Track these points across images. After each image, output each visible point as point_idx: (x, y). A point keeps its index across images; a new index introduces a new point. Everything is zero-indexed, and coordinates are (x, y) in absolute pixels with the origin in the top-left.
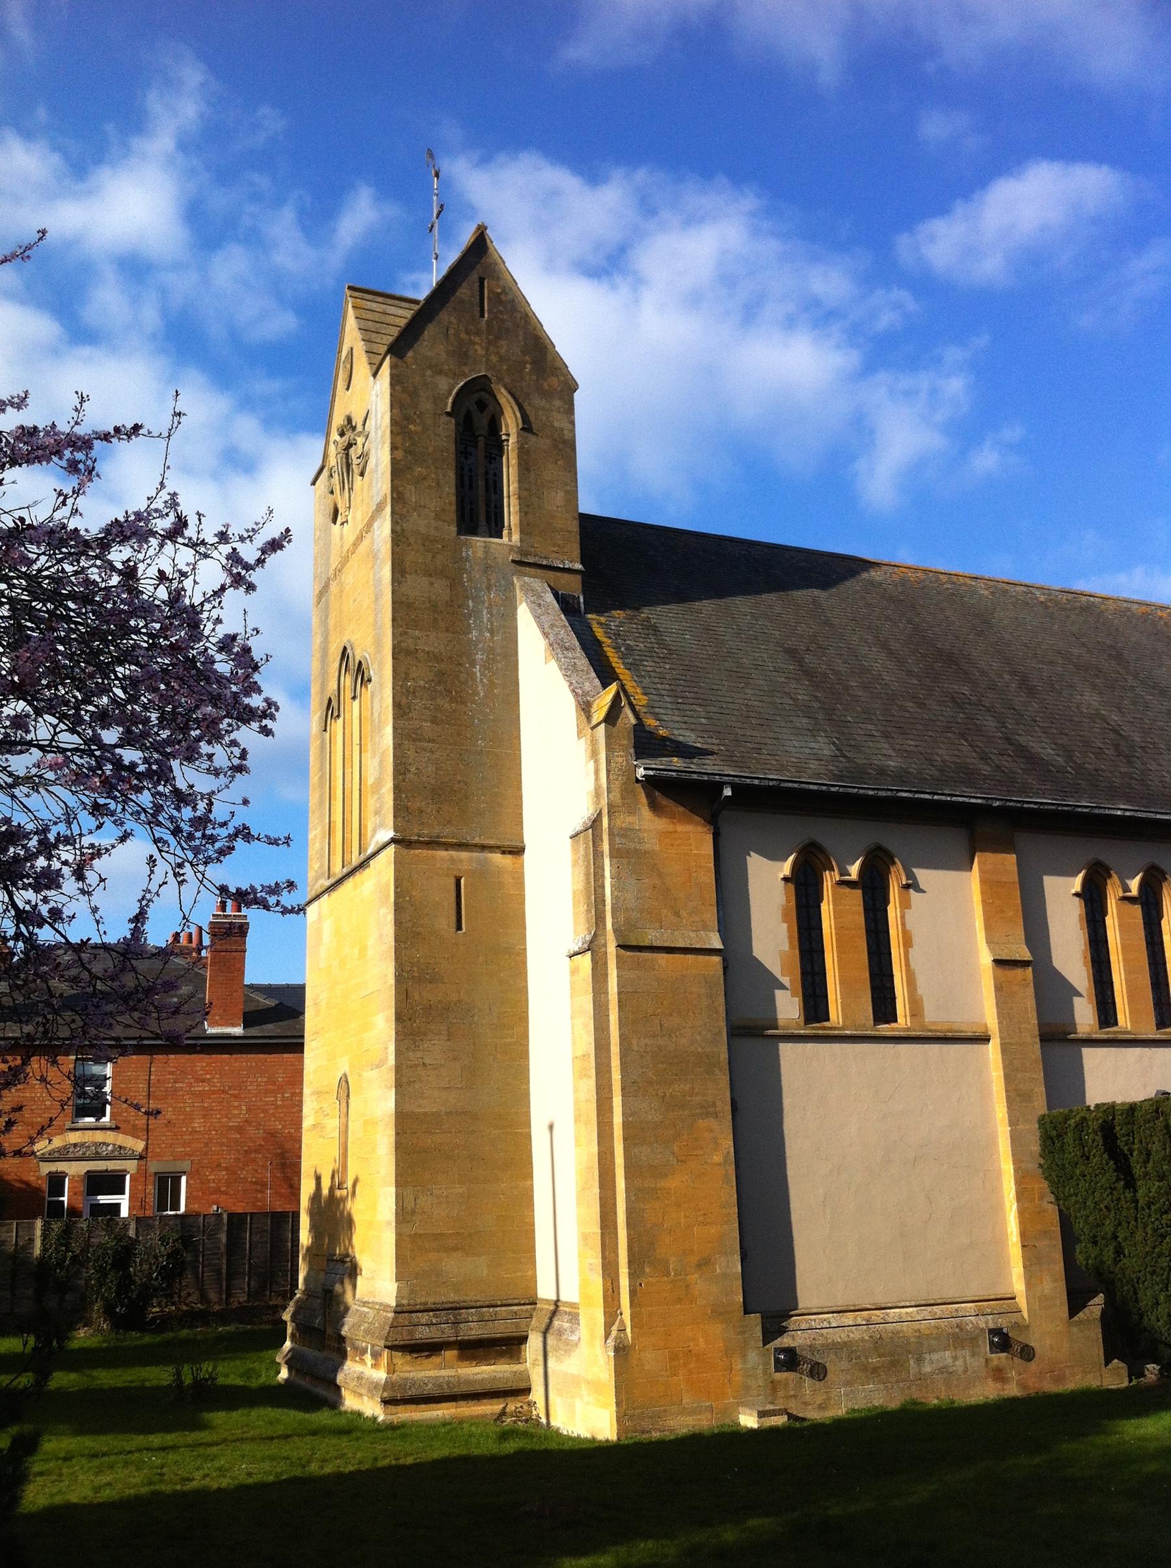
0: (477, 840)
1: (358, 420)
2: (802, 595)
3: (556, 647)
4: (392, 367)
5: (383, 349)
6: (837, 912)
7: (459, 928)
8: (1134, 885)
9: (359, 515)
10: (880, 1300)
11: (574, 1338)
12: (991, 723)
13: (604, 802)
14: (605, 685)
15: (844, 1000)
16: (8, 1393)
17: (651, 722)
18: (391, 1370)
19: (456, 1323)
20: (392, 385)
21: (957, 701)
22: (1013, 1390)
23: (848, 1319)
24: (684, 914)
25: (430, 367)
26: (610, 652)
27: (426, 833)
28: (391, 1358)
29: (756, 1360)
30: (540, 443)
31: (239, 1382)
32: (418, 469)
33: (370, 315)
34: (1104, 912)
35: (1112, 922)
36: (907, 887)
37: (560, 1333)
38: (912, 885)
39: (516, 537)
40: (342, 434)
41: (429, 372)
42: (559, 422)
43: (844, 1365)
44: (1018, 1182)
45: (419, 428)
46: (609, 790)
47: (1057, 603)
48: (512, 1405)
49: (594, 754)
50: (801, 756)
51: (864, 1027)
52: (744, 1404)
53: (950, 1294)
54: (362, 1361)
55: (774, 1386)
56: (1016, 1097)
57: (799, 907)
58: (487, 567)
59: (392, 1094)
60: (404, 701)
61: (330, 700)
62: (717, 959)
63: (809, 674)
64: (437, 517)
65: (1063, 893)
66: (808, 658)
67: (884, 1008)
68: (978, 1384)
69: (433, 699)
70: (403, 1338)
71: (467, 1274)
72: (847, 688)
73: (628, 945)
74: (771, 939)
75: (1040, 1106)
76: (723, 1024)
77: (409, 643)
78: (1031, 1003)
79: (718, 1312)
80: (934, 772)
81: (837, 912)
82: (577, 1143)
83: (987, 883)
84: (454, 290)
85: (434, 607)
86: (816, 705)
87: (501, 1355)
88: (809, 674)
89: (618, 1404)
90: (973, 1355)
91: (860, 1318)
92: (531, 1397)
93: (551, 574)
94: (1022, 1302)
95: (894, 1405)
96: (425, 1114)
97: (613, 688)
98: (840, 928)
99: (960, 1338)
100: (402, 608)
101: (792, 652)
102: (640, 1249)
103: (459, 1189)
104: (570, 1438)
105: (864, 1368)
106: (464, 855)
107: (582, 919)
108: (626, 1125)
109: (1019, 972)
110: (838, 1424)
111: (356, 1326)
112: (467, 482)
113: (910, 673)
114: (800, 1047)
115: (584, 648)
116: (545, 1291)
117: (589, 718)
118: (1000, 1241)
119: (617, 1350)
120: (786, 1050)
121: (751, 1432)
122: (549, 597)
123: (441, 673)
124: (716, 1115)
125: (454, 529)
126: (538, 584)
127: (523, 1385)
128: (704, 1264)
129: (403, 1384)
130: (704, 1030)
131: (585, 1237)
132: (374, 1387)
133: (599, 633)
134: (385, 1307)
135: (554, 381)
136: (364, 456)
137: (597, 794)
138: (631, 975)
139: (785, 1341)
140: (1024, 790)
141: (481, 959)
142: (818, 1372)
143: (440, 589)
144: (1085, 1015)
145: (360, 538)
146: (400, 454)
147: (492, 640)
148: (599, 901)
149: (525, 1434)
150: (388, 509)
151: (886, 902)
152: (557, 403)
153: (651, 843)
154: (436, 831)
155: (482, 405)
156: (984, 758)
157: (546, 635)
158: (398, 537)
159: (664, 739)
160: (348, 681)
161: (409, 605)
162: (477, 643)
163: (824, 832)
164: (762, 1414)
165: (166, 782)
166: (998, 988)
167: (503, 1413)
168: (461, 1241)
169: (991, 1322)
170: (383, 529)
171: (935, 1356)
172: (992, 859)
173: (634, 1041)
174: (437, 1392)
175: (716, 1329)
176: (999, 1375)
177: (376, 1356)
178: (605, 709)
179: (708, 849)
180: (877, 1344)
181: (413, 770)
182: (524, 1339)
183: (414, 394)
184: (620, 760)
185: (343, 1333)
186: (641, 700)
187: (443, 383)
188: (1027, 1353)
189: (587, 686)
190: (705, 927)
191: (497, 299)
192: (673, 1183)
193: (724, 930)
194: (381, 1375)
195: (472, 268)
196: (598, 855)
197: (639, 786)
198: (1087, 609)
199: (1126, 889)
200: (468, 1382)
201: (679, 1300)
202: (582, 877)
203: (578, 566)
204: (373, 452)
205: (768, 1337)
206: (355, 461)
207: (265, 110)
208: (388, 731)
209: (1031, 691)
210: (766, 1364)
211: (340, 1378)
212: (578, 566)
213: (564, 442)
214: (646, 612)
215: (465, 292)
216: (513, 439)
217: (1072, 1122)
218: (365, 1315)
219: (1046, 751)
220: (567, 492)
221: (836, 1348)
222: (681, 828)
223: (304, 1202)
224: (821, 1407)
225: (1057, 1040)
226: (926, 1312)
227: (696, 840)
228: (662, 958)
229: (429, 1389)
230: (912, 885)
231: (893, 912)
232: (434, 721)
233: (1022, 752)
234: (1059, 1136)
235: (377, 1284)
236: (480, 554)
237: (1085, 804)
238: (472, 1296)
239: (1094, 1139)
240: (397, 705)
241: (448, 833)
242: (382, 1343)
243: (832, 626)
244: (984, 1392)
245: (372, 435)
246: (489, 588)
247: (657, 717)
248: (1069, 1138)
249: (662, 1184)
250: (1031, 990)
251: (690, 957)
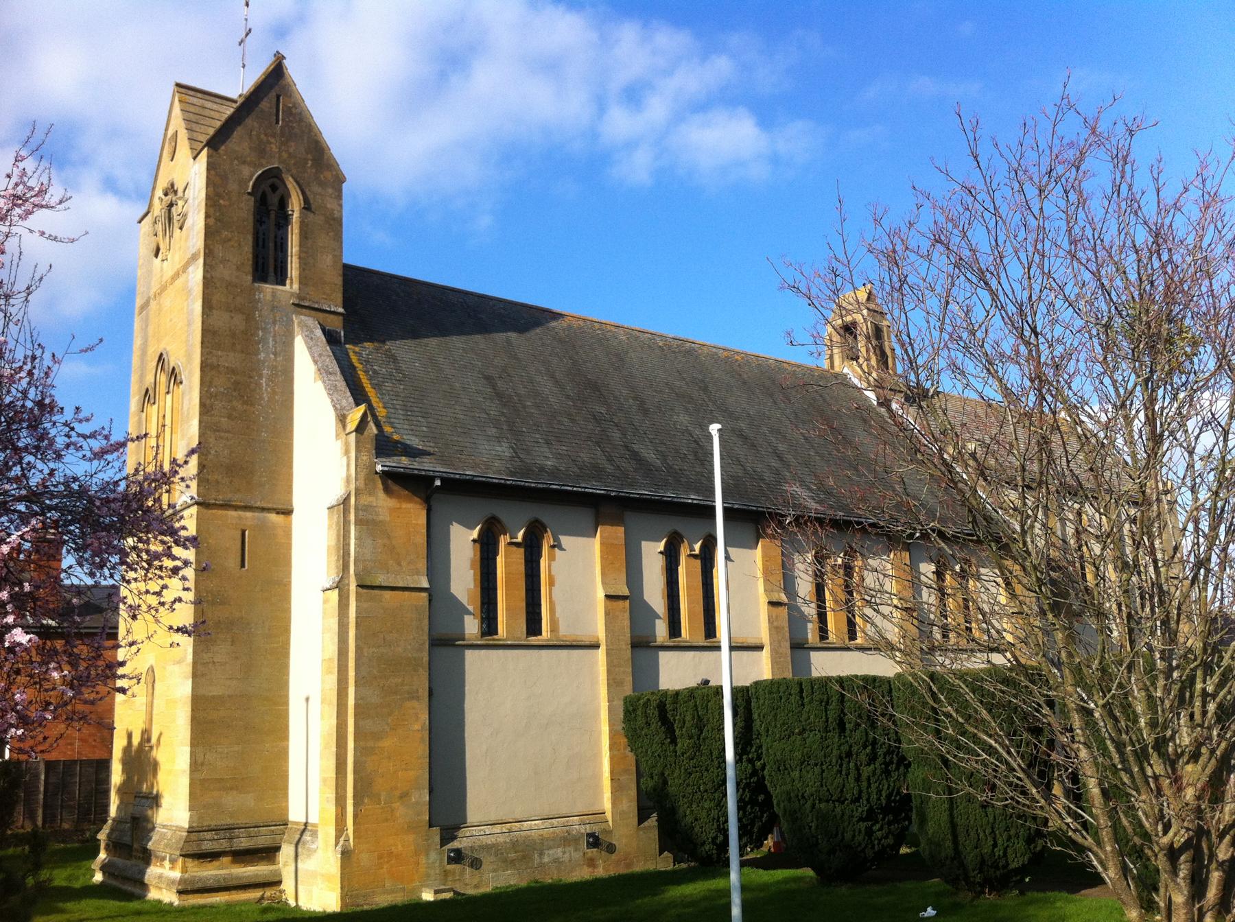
0: (258, 504)
1: (180, 187)
2: (500, 337)
3: (323, 372)
4: (209, 156)
5: (204, 138)
6: (507, 563)
7: (243, 565)
8: (697, 547)
9: (177, 258)
10: (518, 817)
11: (314, 846)
12: (616, 435)
13: (353, 487)
14: (357, 404)
15: (508, 620)
17: (388, 429)
18: (184, 870)
19: (231, 839)
20: (208, 170)
21: (596, 418)
22: (600, 872)
23: (497, 829)
24: (404, 564)
25: (237, 158)
26: (362, 375)
27: (221, 498)
28: (184, 863)
29: (435, 857)
30: (316, 219)
31: (64, 884)
32: (225, 233)
33: (192, 109)
34: (677, 564)
35: (682, 570)
36: (553, 547)
37: (304, 843)
38: (557, 546)
39: (296, 286)
40: (166, 194)
41: (236, 162)
42: (331, 204)
43: (492, 858)
44: (611, 738)
45: (227, 203)
46: (356, 479)
47: (670, 347)
48: (269, 893)
49: (347, 452)
50: (490, 459)
51: (520, 639)
52: (427, 886)
53: (564, 811)
54: (162, 865)
55: (446, 874)
56: (613, 683)
57: (482, 559)
58: (273, 308)
59: (190, 682)
60: (208, 402)
61: (147, 390)
62: (425, 595)
63: (499, 395)
64: (238, 269)
65: (652, 553)
66: (500, 383)
67: (534, 625)
68: (578, 868)
69: (230, 401)
70: (193, 849)
71: (237, 805)
72: (524, 407)
73: (364, 585)
74: (463, 581)
75: (628, 690)
76: (426, 638)
78: (627, 623)
79: (411, 828)
80: (576, 470)
81: (507, 563)
82: (322, 718)
83: (606, 547)
84: (257, 103)
85: (233, 335)
86: (503, 419)
87: (262, 859)
88: (499, 395)
89: (342, 888)
90: (576, 850)
91: (505, 828)
92: (282, 887)
93: (320, 315)
94: (609, 815)
95: (523, 884)
96: (213, 697)
97: (362, 408)
98: (508, 574)
99: (568, 840)
100: (209, 335)
101: (488, 378)
102: (362, 786)
103: (236, 748)
104: (308, 912)
105: (505, 861)
106: (249, 514)
107: (333, 566)
108: (357, 706)
109: (621, 603)
110: (485, 898)
111: (159, 842)
112: (261, 244)
113: (568, 397)
114: (477, 652)
115: (343, 372)
116: (296, 814)
117: (344, 426)
118: (597, 776)
119: (343, 853)
120: (470, 655)
121: (429, 903)
122: (319, 332)
123: (237, 383)
124: (418, 698)
125: (250, 278)
126: (311, 322)
127: (277, 879)
128: (404, 796)
129: (192, 881)
130: (412, 642)
131: (324, 780)
132: (172, 882)
133: (354, 359)
134: (180, 829)
135: (328, 175)
136: (184, 216)
137: (348, 481)
138: (365, 605)
139: (455, 844)
140: (631, 485)
141: (258, 588)
142: (476, 864)
143: (238, 321)
144: (661, 630)
145: (176, 276)
146: (212, 221)
147: (275, 360)
148: (346, 546)
149: (279, 909)
150: (201, 261)
151: (540, 556)
152: (330, 191)
153: (384, 516)
154: (229, 496)
155: (274, 188)
156: (610, 460)
157: (316, 362)
158: (208, 282)
159: (397, 442)
160: (163, 378)
161: (214, 333)
162: (264, 362)
163: (503, 510)
164: (436, 892)
166: (607, 614)
167: (262, 898)
168: (236, 784)
169: (589, 829)
170: (196, 274)
171: (551, 852)
172: (609, 529)
173: (365, 650)
174: (216, 885)
175: (411, 838)
176: (591, 863)
177: (173, 861)
178: (356, 423)
179: (423, 520)
180: (514, 845)
181: (213, 452)
182: (278, 849)
183: (224, 178)
184: (364, 458)
185: (150, 845)
186: (381, 412)
187: (246, 171)
188: (611, 849)
189: (344, 403)
190: (418, 573)
191: (289, 112)
192: (387, 743)
193: (430, 575)
194: (176, 874)
195: (271, 87)
196: (346, 523)
197: (377, 477)
198: (689, 352)
199: (692, 549)
200: (238, 878)
201: (387, 820)
202: (334, 536)
203: (341, 310)
204: (190, 215)
205: (444, 842)
206: (176, 218)
208: (195, 423)
209: (645, 412)
210: (441, 860)
211: (147, 879)
212: (341, 310)
213: (334, 219)
214: (389, 345)
215: (265, 105)
216: (296, 216)
217: (641, 702)
218: (165, 834)
219: (650, 455)
220: (335, 256)
221: (487, 848)
222: (404, 506)
223: (117, 753)
224: (476, 886)
225: (642, 645)
226: (548, 823)
227: (414, 514)
228: (387, 594)
229: (210, 883)
230: (557, 546)
231: (543, 563)
232: (230, 417)
233: (636, 456)
234: (634, 710)
235: (174, 812)
236: (269, 297)
237: (669, 495)
238: (242, 820)
239: (653, 713)
240: (202, 405)
241: (237, 499)
242: (178, 853)
243: (518, 359)
244: (583, 874)
245: (190, 201)
246: (274, 323)
247: (392, 425)
248: (639, 712)
249: (381, 744)
250: (627, 615)
251: (407, 593)
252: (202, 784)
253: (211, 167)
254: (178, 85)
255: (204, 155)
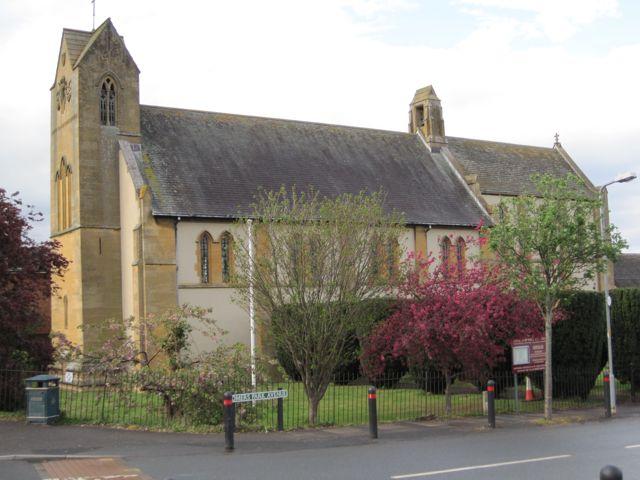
16: (3, 461)
77: (85, 164)
85: (92, 152)
100: (82, 153)
143: (94, 146)
150: (78, 120)
165: (35, 363)
207: (54, 345)
208: (78, 192)
212: (139, 135)
252: (482, 398)
253: (80, 75)
254: (65, 30)
255: (77, 70)
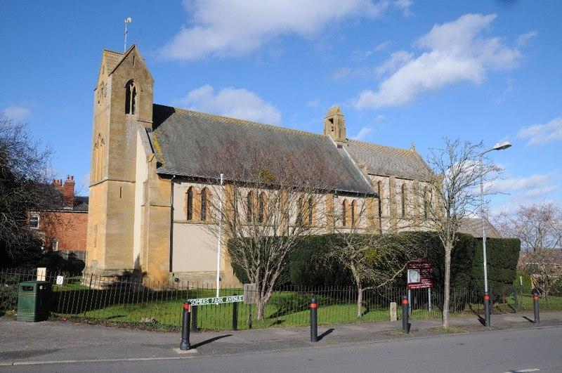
30: (145, 94)
67: (203, 218)
101: (197, 142)
143: (120, 127)
160: (100, 141)
170: (109, 112)
253: (113, 79)
